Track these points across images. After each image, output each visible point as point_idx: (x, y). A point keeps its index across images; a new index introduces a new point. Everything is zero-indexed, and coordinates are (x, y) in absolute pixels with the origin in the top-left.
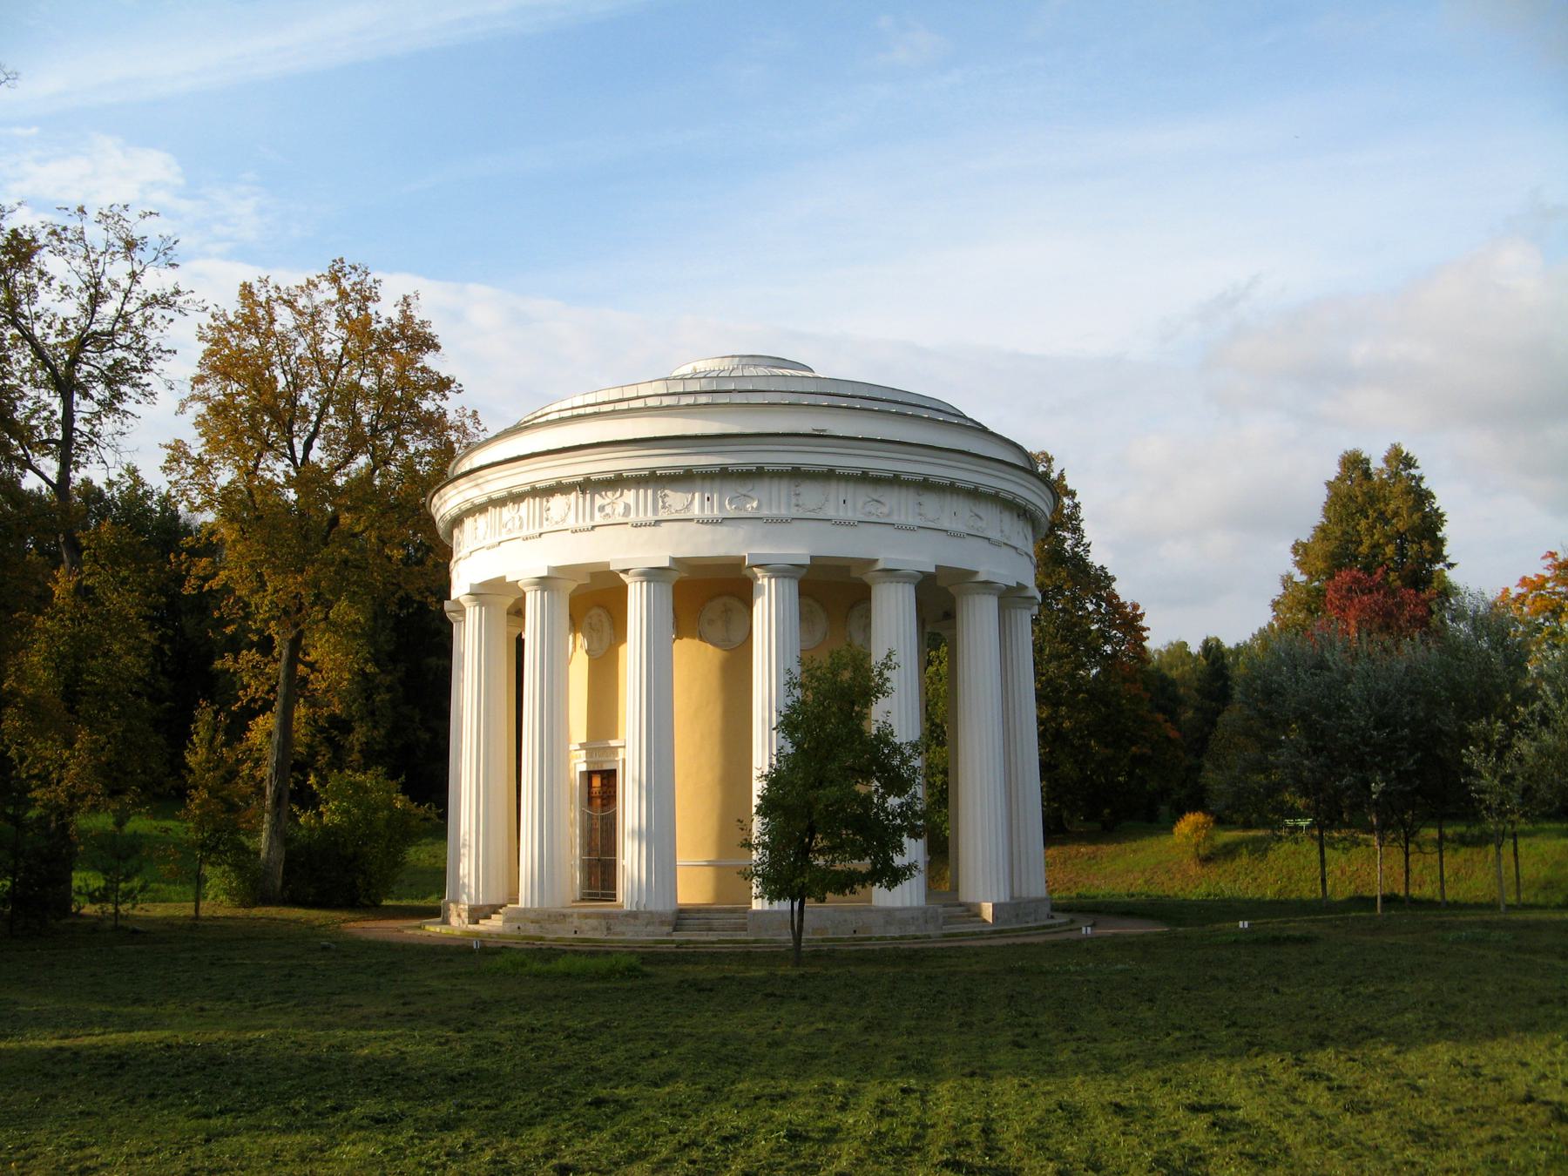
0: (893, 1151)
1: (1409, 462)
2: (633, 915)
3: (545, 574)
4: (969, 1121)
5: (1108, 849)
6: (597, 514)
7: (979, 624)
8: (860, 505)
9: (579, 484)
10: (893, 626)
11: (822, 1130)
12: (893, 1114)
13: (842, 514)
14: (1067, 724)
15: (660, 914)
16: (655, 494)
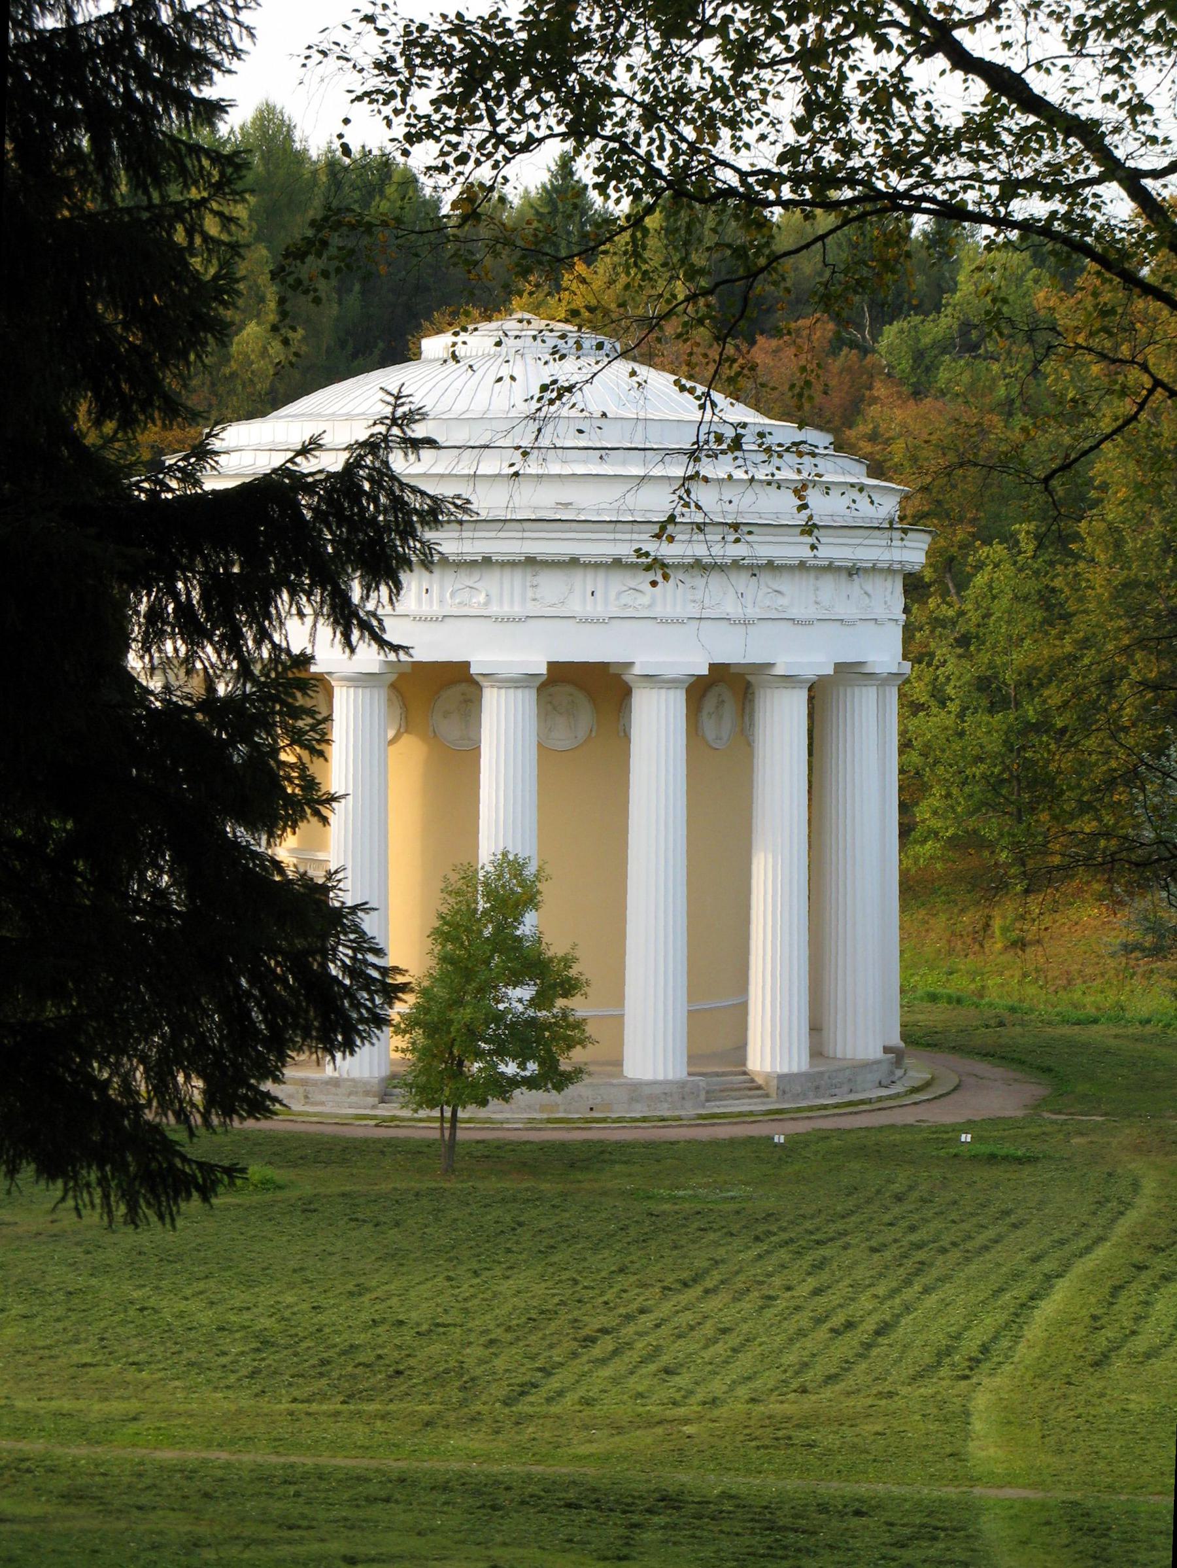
8: (612, 595)
15: (365, 1083)
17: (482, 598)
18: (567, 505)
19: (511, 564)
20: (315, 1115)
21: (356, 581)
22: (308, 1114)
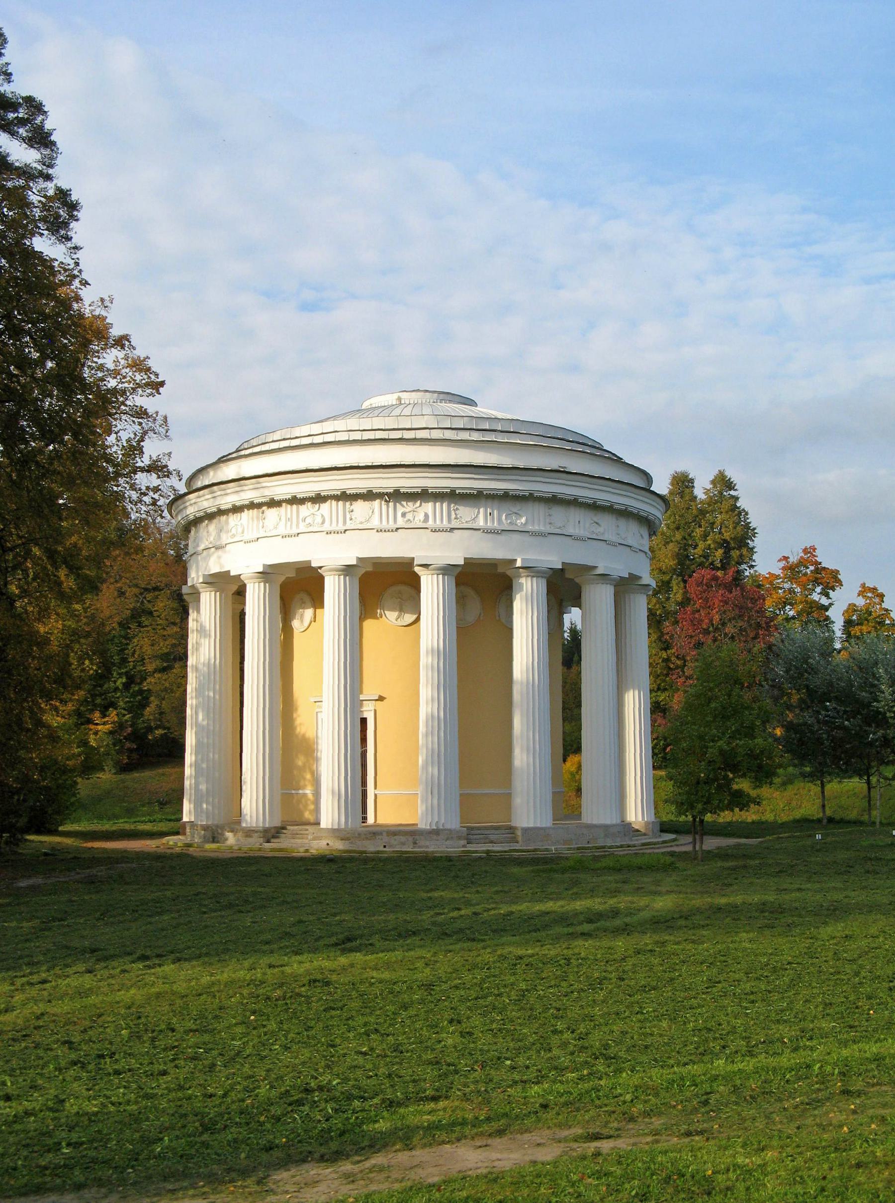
1: (730, 485)
17: (523, 520)
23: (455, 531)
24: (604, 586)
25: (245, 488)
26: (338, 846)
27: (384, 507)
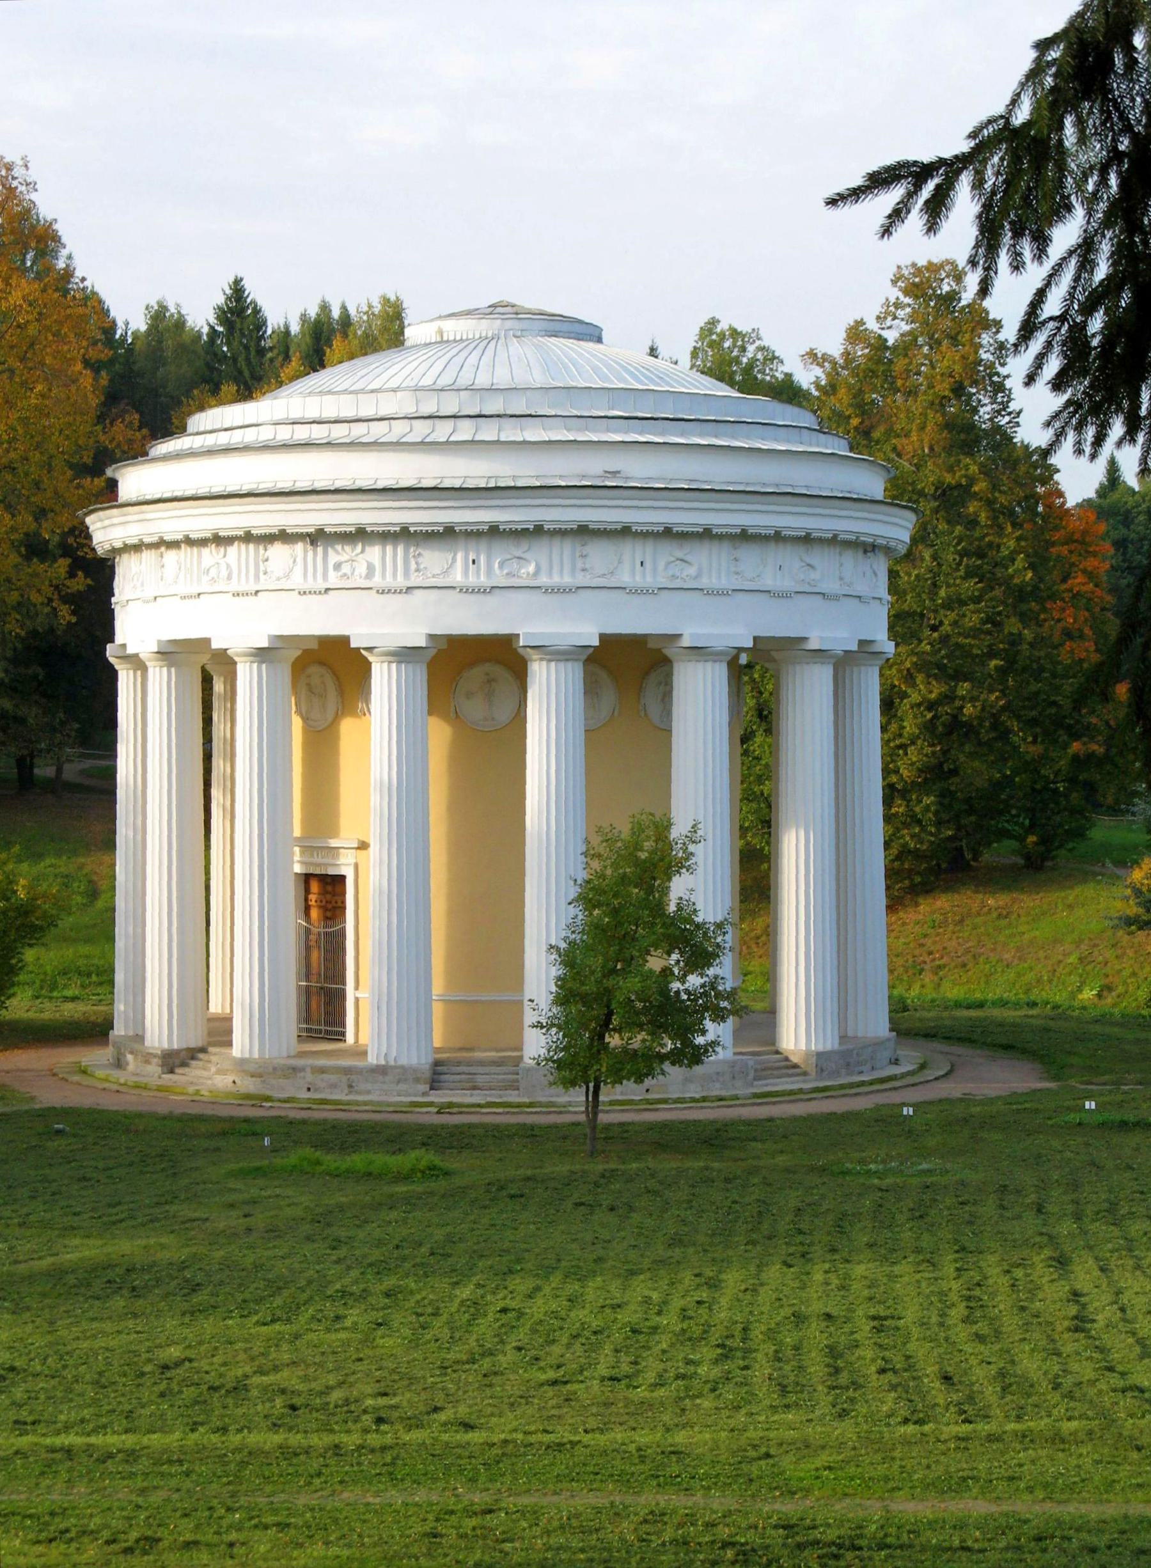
0: (690, 1339)
2: (381, 1071)
3: (265, 644)
4: (736, 1322)
5: (1029, 902)
6: (332, 573)
7: (808, 705)
8: (661, 565)
9: (308, 535)
10: (700, 707)
11: (649, 1328)
12: (691, 1318)
13: (641, 579)
14: (969, 710)
16: (406, 552)
17: (531, 568)
18: (615, 474)
19: (561, 533)
20: (365, 1103)
21: (1143, 433)
22: (357, 1103)
23: (416, 592)
24: (700, 665)
25: (129, 518)
26: (249, 1085)
27: (310, 554)
